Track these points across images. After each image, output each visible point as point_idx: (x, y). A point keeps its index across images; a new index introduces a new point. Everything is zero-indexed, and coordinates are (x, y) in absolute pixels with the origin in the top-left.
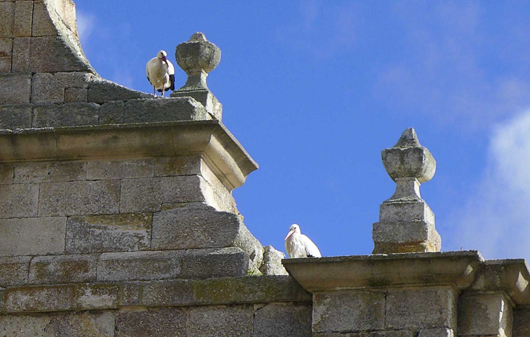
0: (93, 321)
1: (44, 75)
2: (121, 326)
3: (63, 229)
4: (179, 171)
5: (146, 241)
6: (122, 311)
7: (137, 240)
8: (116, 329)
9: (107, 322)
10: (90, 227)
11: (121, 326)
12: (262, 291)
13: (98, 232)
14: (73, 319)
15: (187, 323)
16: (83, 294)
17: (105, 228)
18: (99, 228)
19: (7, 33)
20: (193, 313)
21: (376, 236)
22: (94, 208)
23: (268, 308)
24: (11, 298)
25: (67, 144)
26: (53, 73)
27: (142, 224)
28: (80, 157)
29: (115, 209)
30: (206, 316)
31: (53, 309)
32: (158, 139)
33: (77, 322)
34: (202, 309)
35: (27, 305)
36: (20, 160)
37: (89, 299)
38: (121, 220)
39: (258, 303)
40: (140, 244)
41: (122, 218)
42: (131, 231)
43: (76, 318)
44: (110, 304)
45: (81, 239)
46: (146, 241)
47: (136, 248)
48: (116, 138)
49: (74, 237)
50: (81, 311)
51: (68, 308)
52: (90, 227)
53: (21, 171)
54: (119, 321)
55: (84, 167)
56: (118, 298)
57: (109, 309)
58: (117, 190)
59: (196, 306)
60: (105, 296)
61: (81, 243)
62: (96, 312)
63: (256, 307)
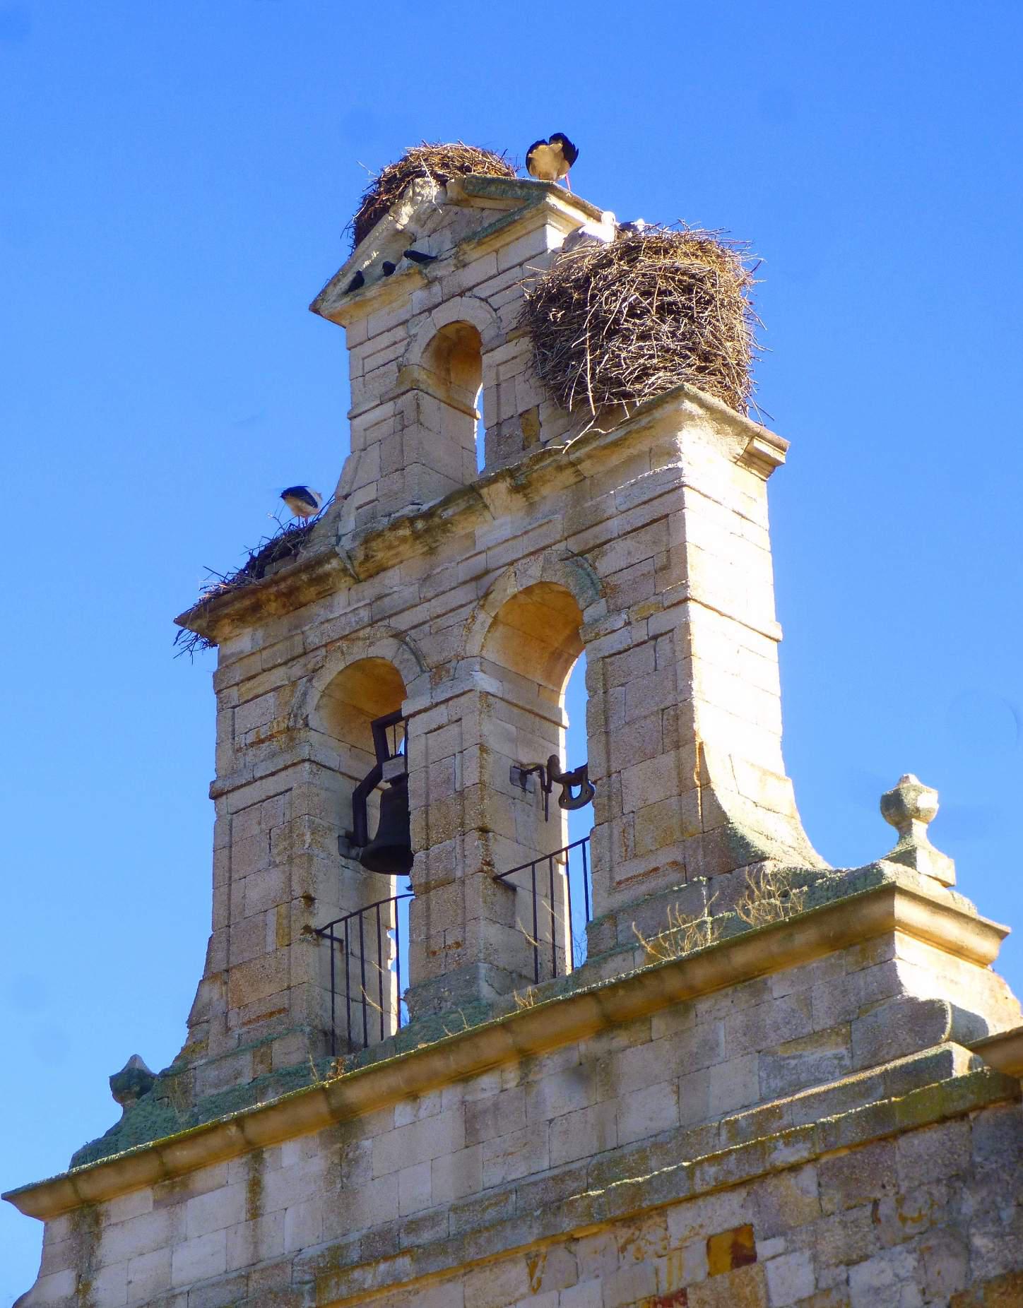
0: (793, 1181)
1: (722, 877)
2: (824, 1180)
3: (756, 1069)
4: (873, 959)
5: (847, 1062)
6: (824, 1160)
7: (836, 1062)
8: (819, 1185)
9: (808, 1177)
10: (784, 1059)
11: (824, 1180)
12: (973, 1092)
13: (793, 1062)
14: (772, 1183)
15: (898, 1158)
16: (776, 1148)
17: (801, 1056)
18: (794, 1058)
19: (677, 835)
20: (902, 1142)
21: (211, 788)
22: (785, 1032)
23: (986, 1114)
24: (698, 1174)
25: (741, 958)
26: (730, 872)
27: (840, 1039)
28: (762, 971)
29: (808, 1029)
30: (916, 1142)
31: (745, 1177)
32: (832, 926)
33: (776, 1187)
34: (910, 1134)
35: (716, 1179)
36: (696, 993)
37: (784, 1155)
38: (817, 1041)
39: (974, 1109)
40: (841, 1066)
41: (816, 1037)
42: (829, 1051)
43: (774, 1181)
44: (806, 1154)
45: (775, 1077)
46: (847, 1062)
47: (837, 1074)
48: (791, 935)
49: (768, 1076)
50: (777, 1172)
51: (760, 1171)
52: (784, 1059)
53: (703, 1006)
54: (820, 1175)
55: (769, 983)
56: (814, 1145)
57: (809, 1161)
58: (807, 1002)
59: (904, 1132)
60: (800, 1145)
61: (776, 1083)
62: (794, 1168)
63: (972, 1116)
